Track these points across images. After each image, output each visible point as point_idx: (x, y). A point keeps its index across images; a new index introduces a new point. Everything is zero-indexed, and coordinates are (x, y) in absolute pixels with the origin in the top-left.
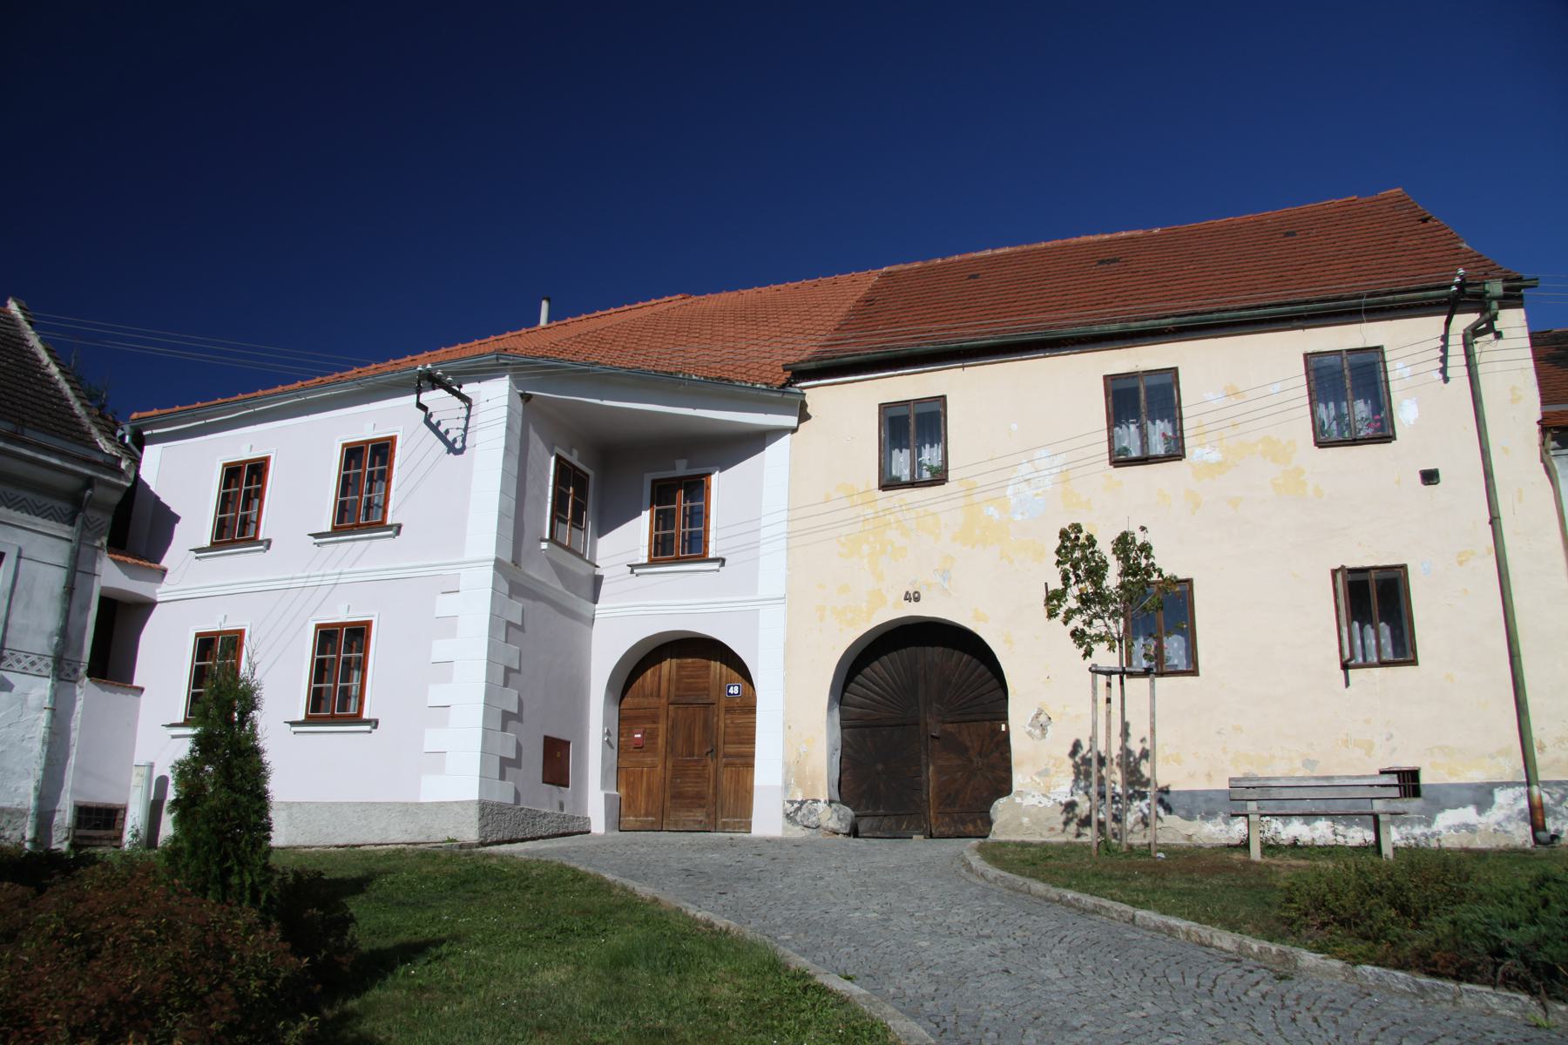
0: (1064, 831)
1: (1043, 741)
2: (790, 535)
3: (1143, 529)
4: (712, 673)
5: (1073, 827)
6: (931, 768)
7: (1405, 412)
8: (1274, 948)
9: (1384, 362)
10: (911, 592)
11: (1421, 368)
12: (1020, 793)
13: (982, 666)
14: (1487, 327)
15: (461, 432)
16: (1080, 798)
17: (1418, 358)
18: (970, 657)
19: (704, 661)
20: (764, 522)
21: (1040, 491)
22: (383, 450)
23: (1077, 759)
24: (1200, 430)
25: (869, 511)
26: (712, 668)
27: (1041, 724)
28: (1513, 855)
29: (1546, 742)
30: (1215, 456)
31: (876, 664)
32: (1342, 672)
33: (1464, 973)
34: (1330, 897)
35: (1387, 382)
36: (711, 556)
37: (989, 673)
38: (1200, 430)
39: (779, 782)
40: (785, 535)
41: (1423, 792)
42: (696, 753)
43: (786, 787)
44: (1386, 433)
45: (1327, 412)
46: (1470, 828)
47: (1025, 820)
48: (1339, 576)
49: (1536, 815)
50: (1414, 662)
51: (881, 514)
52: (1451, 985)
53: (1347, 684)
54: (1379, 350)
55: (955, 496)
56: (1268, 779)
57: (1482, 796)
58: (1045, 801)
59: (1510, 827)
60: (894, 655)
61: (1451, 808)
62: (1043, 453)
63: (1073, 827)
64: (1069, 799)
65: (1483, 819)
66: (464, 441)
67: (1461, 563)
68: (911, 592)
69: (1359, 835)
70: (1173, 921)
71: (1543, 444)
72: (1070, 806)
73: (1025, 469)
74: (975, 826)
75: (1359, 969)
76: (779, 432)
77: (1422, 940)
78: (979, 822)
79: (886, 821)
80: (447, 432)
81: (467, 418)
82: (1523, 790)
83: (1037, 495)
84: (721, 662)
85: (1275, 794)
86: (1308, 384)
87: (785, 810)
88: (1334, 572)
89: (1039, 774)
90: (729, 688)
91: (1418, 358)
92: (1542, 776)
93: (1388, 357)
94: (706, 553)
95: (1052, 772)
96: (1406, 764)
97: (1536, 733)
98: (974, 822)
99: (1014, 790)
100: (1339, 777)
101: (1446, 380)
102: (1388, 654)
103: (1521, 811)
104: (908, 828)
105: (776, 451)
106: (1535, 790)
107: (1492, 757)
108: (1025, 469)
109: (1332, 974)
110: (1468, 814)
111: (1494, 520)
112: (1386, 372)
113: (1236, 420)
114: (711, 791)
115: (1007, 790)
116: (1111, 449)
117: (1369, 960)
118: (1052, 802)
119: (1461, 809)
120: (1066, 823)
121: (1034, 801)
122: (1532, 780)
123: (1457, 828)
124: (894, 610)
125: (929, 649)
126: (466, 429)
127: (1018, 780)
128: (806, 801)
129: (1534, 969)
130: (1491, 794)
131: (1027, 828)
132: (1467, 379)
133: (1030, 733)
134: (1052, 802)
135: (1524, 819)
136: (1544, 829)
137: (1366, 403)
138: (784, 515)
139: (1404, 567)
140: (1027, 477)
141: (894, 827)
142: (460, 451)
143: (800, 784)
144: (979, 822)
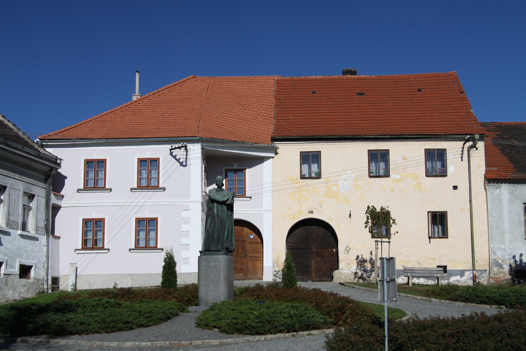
0: (354, 280)
1: (348, 255)
2: (273, 191)
3: (388, 207)
4: (244, 231)
5: (357, 279)
6: (313, 261)
7: (450, 169)
8: (428, 298)
9: (446, 154)
10: (311, 211)
11: (456, 156)
12: (341, 269)
13: (328, 232)
14: (474, 146)
15: (184, 160)
16: (358, 271)
17: (455, 153)
18: (325, 230)
19: (241, 228)
20: (264, 186)
21: (348, 183)
22: (155, 162)
23: (358, 260)
24: (394, 169)
25: (297, 185)
26: (244, 230)
27: (348, 250)
28: (469, 287)
29: (478, 260)
30: (398, 177)
31: (297, 231)
32: (429, 239)
33: (456, 300)
34: (435, 291)
35: (446, 159)
36: (247, 196)
37: (330, 234)
38: (394, 169)
39: (271, 265)
40: (271, 191)
41: (448, 272)
42: (240, 256)
43: (273, 267)
44: (445, 175)
45: (429, 164)
46: (458, 281)
47: (343, 277)
48: (430, 214)
49: (474, 278)
50: (447, 238)
51: (301, 187)
52: (454, 302)
53: (430, 243)
54: (445, 150)
55: (323, 183)
56: (413, 268)
57: (462, 273)
58: (348, 271)
59: (468, 281)
60: (302, 228)
61: (454, 276)
62: (349, 172)
63: (357, 279)
64: (355, 271)
65: (462, 279)
66: (186, 162)
67: (461, 212)
68: (311, 211)
69: (431, 282)
70: (408, 295)
71: (485, 181)
72: (356, 273)
73: (344, 176)
74: (326, 278)
75: (441, 300)
76: (268, 158)
77: (451, 296)
78: (327, 277)
79: (300, 276)
80: (179, 159)
81: (187, 155)
82: (472, 272)
83: (347, 184)
84: (248, 228)
85: (414, 272)
86: (425, 158)
87: (273, 273)
88: (428, 212)
89: (347, 264)
90: (250, 236)
91: (455, 153)
92: (476, 268)
93: (447, 152)
94: (245, 195)
95: (350, 264)
96: (443, 264)
97: (476, 257)
98: (326, 277)
99: (340, 269)
100: (429, 268)
101: (462, 160)
102: (441, 235)
103: (471, 277)
104: (306, 278)
105: (267, 164)
106: (474, 272)
107: (465, 263)
108: (344, 176)
109: (437, 301)
110: (458, 278)
111: (470, 201)
112: (446, 157)
113: (405, 167)
114: (245, 268)
115: (337, 268)
116: (369, 173)
117: (443, 299)
118: (350, 272)
119: (456, 276)
120: (355, 278)
121: (346, 272)
122: (474, 269)
123: (455, 281)
124: (306, 216)
125: (313, 227)
126: (186, 159)
127: (341, 265)
128: (280, 271)
129: (465, 299)
130: (464, 272)
131: (344, 279)
132: (467, 160)
133: (344, 253)
134: (350, 272)
135: (471, 279)
136: (476, 282)
137: (440, 162)
138: (271, 185)
139: (446, 212)
140: (345, 179)
141: (302, 278)
142: (186, 166)
143: (277, 266)
144: (327, 277)
